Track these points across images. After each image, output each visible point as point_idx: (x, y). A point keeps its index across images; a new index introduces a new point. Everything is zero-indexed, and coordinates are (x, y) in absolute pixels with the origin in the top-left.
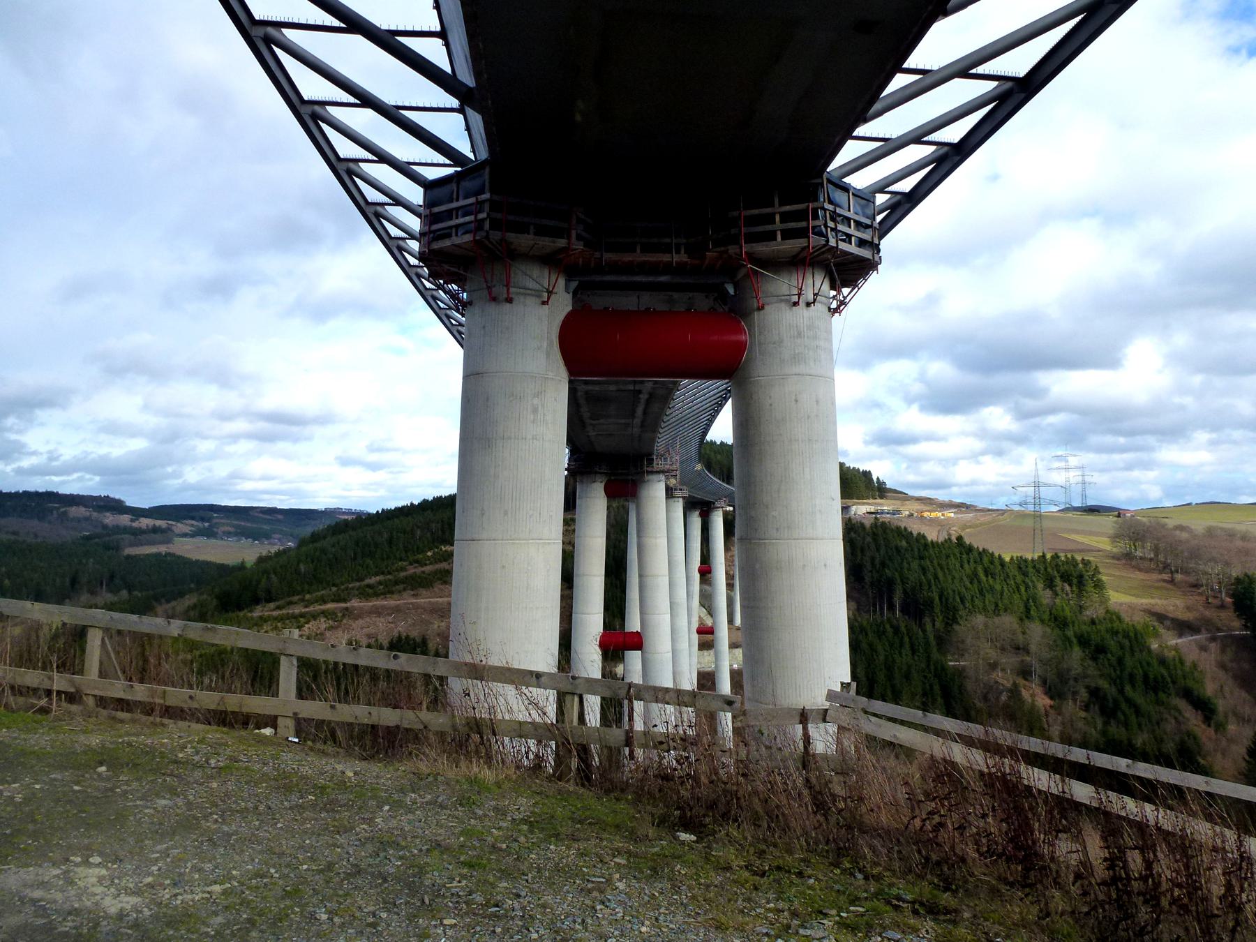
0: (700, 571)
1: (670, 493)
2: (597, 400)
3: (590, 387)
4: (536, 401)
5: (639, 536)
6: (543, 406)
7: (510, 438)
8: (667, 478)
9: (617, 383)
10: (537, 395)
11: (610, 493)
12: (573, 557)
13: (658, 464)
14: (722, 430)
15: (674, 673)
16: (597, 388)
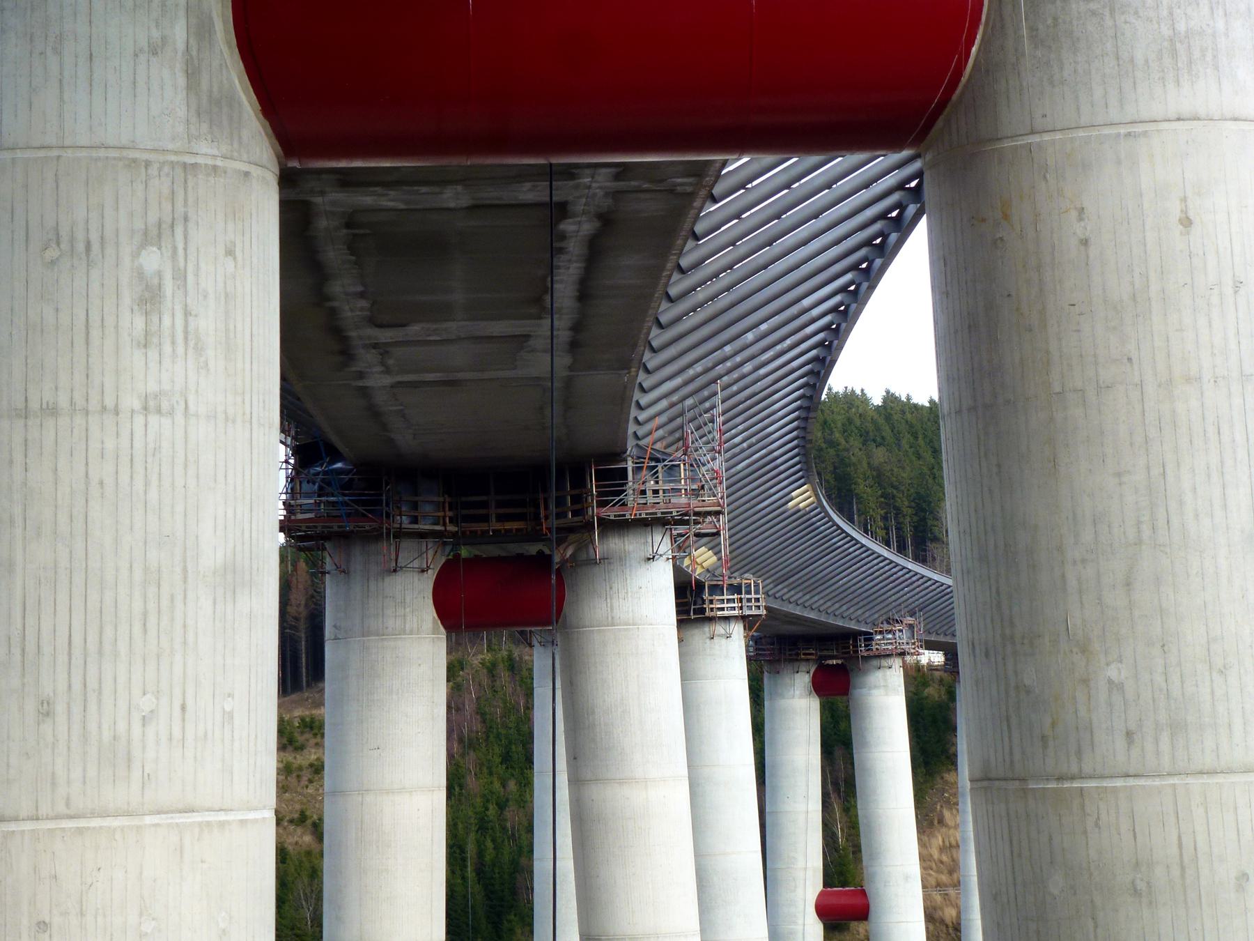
0: (823, 910)
1: (692, 602)
2: (399, 248)
3: (366, 199)
4: (152, 260)
5: (576, 781)
6: (180, 277)
7: (52, 411)
8: (681, 547)
9: (466, 179)
10: (152, 236)
11: (459, 610)
12: (315, 874)
13: (643, 491)
14: (893, 350)
15: (699, 855)
16: (391, 200)
